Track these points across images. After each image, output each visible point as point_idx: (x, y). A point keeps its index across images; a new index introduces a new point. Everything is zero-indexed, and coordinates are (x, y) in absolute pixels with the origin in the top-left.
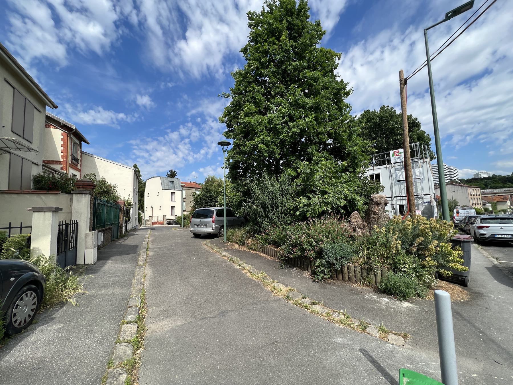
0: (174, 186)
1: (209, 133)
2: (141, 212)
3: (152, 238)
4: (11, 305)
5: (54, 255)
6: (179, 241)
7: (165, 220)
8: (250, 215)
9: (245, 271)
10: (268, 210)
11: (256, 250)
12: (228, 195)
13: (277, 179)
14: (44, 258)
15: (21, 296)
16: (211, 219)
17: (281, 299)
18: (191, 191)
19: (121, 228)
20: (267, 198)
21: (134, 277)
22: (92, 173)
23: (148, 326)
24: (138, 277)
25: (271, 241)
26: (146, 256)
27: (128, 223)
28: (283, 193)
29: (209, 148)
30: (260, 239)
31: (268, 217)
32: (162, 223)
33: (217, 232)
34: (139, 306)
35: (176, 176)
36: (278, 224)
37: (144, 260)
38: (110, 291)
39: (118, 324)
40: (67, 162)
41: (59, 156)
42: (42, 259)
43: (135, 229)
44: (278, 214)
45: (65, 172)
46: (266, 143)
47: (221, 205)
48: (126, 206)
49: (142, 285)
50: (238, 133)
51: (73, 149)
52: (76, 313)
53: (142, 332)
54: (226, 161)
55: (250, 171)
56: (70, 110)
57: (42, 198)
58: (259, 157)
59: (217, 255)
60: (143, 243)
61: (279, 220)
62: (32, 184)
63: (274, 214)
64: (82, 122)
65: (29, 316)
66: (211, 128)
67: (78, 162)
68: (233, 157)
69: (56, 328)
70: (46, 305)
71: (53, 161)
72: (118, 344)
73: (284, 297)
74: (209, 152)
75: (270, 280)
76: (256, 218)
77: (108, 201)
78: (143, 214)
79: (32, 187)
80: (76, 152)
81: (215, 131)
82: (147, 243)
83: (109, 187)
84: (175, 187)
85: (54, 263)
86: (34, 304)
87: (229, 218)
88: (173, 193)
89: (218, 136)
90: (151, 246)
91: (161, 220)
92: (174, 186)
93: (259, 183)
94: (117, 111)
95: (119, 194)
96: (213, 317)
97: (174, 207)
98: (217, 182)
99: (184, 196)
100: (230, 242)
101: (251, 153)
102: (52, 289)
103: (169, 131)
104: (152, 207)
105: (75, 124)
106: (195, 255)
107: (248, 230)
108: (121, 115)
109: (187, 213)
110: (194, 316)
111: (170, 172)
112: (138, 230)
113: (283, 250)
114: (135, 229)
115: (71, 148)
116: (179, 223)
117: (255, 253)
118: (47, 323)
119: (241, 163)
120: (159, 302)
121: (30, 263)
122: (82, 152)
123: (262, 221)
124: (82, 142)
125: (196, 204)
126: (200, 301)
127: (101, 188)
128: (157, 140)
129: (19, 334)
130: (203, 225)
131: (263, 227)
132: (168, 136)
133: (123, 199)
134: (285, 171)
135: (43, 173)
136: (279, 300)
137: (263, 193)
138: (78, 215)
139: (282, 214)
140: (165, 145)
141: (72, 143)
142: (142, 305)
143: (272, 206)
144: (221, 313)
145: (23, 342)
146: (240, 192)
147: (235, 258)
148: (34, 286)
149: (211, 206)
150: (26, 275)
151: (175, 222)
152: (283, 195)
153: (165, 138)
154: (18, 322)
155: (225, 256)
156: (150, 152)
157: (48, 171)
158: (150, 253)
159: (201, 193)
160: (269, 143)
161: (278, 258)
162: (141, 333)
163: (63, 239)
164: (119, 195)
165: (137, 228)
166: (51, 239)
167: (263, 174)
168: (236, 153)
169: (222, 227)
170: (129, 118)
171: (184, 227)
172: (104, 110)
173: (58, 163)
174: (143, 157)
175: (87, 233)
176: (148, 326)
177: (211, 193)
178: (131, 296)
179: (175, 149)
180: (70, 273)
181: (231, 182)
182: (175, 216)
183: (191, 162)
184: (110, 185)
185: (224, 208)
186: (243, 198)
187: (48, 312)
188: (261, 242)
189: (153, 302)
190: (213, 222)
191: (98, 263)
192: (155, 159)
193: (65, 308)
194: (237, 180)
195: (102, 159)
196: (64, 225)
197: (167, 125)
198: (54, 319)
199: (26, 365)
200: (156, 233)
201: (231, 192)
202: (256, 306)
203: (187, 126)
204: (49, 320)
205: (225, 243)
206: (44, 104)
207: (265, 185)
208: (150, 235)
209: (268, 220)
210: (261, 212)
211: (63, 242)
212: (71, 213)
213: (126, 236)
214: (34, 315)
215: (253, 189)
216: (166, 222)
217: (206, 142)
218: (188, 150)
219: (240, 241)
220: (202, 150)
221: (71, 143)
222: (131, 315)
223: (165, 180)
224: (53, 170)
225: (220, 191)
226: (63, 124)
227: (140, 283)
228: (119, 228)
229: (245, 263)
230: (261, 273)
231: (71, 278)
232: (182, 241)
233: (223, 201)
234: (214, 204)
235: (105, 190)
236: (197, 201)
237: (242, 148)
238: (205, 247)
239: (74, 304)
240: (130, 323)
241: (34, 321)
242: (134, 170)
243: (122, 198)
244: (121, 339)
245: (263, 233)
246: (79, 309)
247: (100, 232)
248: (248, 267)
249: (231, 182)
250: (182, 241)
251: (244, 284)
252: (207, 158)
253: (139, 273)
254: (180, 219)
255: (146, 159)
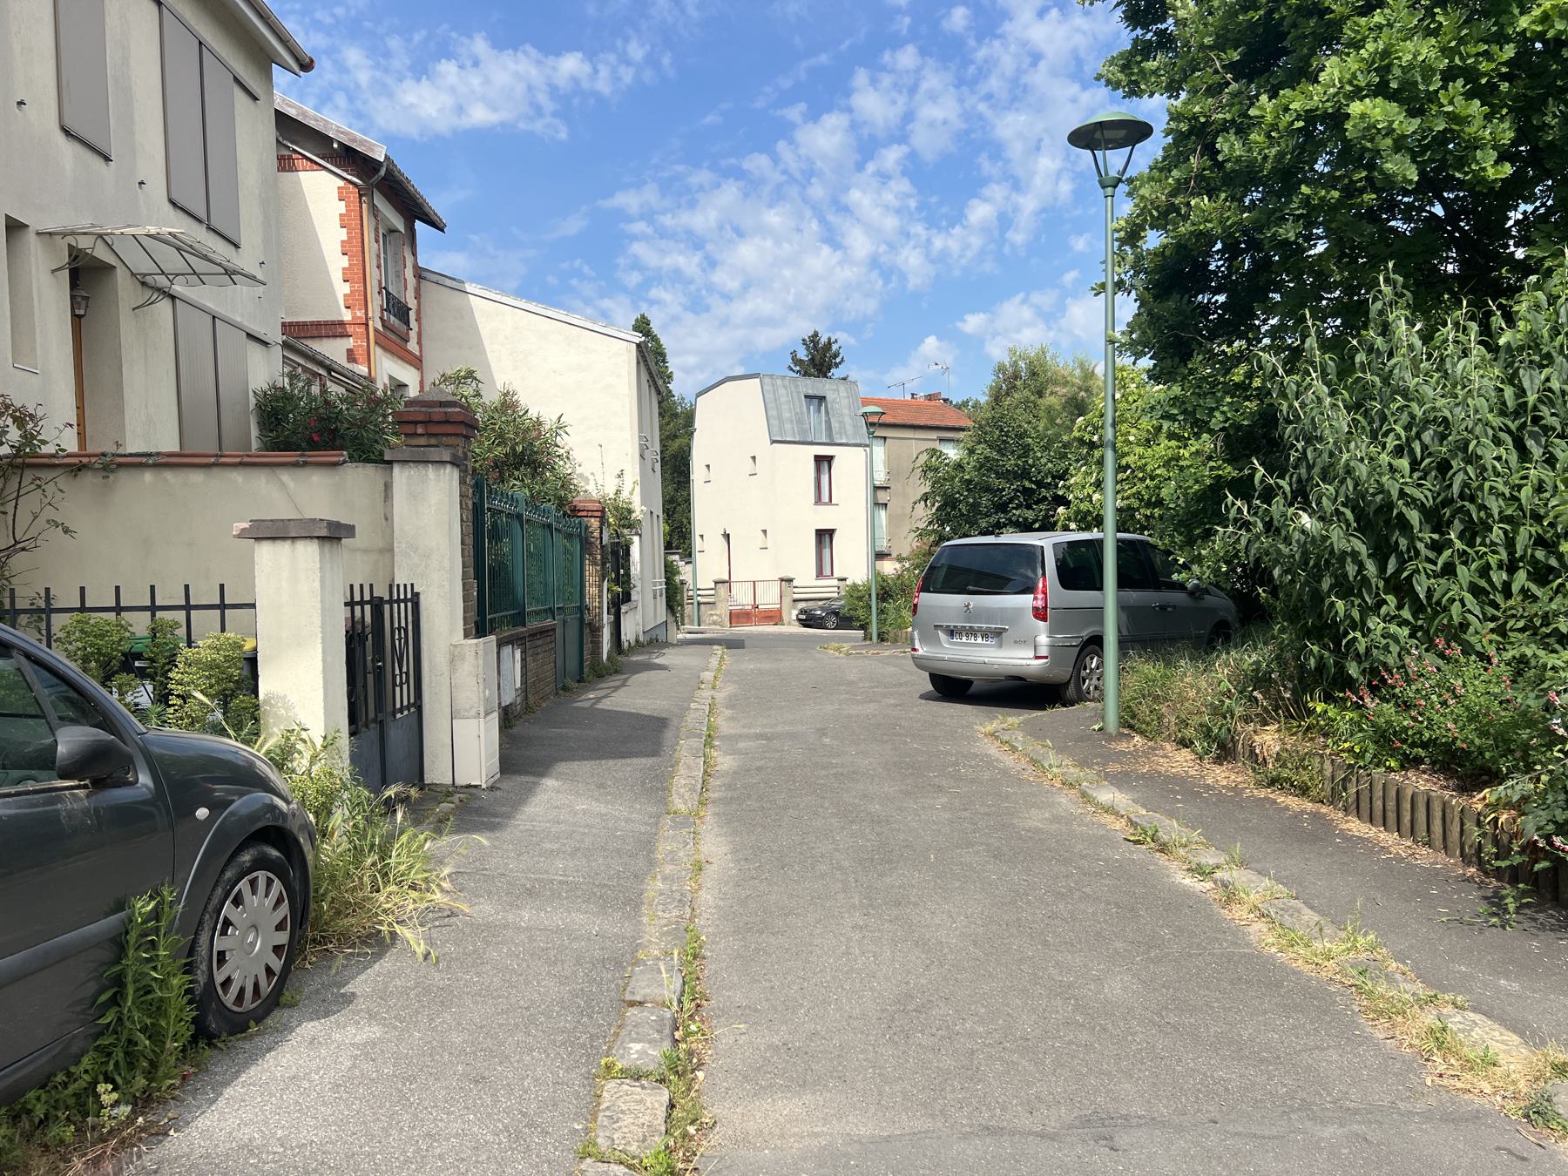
0: (828, 422)
1: (1018, 93)
2: (676, 557)
3: (730, 689)
4: (207, 916)
5: (338, 731)
6: (855, 710)
7: (787, 601)
8: (1276, 572)
9: (1239, 913)
10: (1403, 543)
11: (1313, 793)
12: (1130, 459)
13: (1487, 332)
14: (304, 741)
15: (237, 889)
16: (1026, 601)
17: (1488, 1114)
18: (915, 447)
19: (596, 631)
20: (1404, 463)
21: (652, 863)
22: (460, 367)
23: (715, 1110)
24: (668, 869)
25: (1424, 745)
26: (705, 772)
27: (624, 608)
28: (1524, 425)
29: (1017, 185)
30: (1344, 727)
31: (1402, 588)
32: (774, 617)
33: (1063, 673)
34: (675, 1007)
35: (837, 365)
36: (1481, 635)
37: (692, 790)
38: (554, 917)
39: (589, 1072)
40: (367, 325)
41: (337, 301)
42: (300, 746)
43: (653, 642)
44: (1484, 571)
45: (362, 369)
46: (1408, 85)
47: (1083, 519)
48: (609, 525)
49: (688, 910)
50: (1202, 47)
51: (385, 259)
52: (427, 991)
53: (691, 1130)
54: (1123, 242)
55: (1277, 297)
56: (364, 77)
57: (283, 485)
58: (1350, 191)
59: (1066, 801)
60: (689, 709)
61: (1491, 611)
62: (254, 432)
63: (1449, 570)
64: (413, 131)
65: (269, 971)
66: (1028, 60)
67: (407, 323)
68: (1164, 216)
69: (358, 1039)
70: (322, 937)
71: (318, 324)
72: (589, 1160)
73: (1511, 1104)
74: (1016, 209)
75: (1408, 986)
76: (1318, 597)
77: (533, 501)
78: (689, 567)
79: (255, 444)
80: (398, 276)
81: (1054, 73)
82: (707, 708)
83: (534, 434)
84: (835, 425)
85: (342, 766)
86: (280, 927)
87: (1134, 596)
88: (823, 462)
89: (1074, 100)
90: (724, 725)
91: (769, 598)
92: (828, 422)
93: (1346, 368)
94: (552, 48)
95: (579, 470)
96: (1042, 1136)
97: (831, 532)
98: (1066, 383)
99: (880, 478)
100: (1142, 733)
101: (1287, 176)
102: (340, 875)
103: (794, 113)
104: (727, 537)
105: (387, 139)
106: (940, 788)
107: (1257, 670)
108: (571, 64)
109: (898, 566)
110: (938, 1107)
111: (808, 348)
112: (667, 644)
113: (1509, 805)
114: (653, 642)
115: (379, 256)
116: (858, 619)
117: (1303, 812)
118: (327, 1015)
119: (1219, 246)
120: (766, 1005)
121: (258, 753)
122: (420, 274)
123: (1356, 614)
124: (418, 225)
125: (942, 517)
126: (971, 1035)
127: (501, 438)
128: (738, 174)
129: (239, 1036)
130: (980, 630)
131: (1362, 650)
132: (791, 141)
133: (595, 495)
134: (1549, 273)
135: (286, 380)
136: (1477, 1116)
137: (1374, 435)
138: (416, 560)
139: (1512, 569)
140: (778, 197)
141: (381, 231)
142: (686, 1006)
143: (1435, 519)
144: (1086, 1122)
145: (253, 1071)
146: (1211, 432)
147: (1171, 829)
148: (275, 853)
149: (1026, 527)
150: (246, 803)
151: (836, 614)
152: (1530, 443)
153: (776, 160)
154: (234, 990)
155: (1110, 810)
156: (709, 247)
157: (305, 369)
158: (725, 762)
159: (971, 452)
160: (1427, 80)
161: (1473, 856)
162: (685, 1135)
163: (369, 664)
164: (581, 475)
165: (662, 638)
166: (324, 661)
167: (1379, 305)
168: (1187, 181)
169: (1094, 643)
170: (604, 72)
171: (882, 638)
172: (495, 52)
173: (335, 330)
174: (677, 277)
175: (455, 646)
176: (715, 1110)
177: (1027, 450)
178: (641, 955)
179: (831, 218)
180: (399, 815)
181: (1155, 376)
182: (835, 582)
183: (914, 282)
184: (539, 423)
185: (1109, 536)
186: (1229, 471)
187: (330, 967)
188: (1351, 750)
189: (738, 997)
190: (1040, 614)
191: (504, 785)
192: (733, 285)
193: (385, 964)
194: (1186, 357)
195: (498, 298)
196: (367, 603)
197: (786, 83)
198: (351, 1002)
199: (264, 1163)
200: (747, 663)
201: (1147, 443)
202: (1309, 1124)
203: (892, 71)
204: (335, 1002)
205: (1110, 738)
206: (263, 59)
207: (1386, 380)
208: (719, 670)
209: (1400, 607)
210: (1355, 554)
211: (370, 678)
212: (391, 550)
213: (616, 672)
214: (286, 970)
215: (1303, 405)
216: (795, 612)
217: (997, 150)
218: (898, 212)
219: (1207, 733)
220: (974, 202)
221: (376, 230)
222: (639, 1041)
223: (782, 391)
224: (321, 364)
225: (1081, 441)
226: (339, 143)
227: (677, 896)
228: (587, 631)
229: (1243, 864)
230: (1343, 935)
231: (404, 838)
232: (871, 709)
233: (1096, 497)
234: (1047, 517)
235: (519, 449)
236: (949, 503)
237: (1229, 146)
238: (993, 749)
239: (420, 950)
240: (637, 1076)
241: (287, 996)
242: (638, 346)
243: (591, 488)
244: (599, 1141)
245: (1364, 691)
246: (437, 976)
247: (508, 643)
248: (1255, 887)
249: (1155, 376)
250: (871, 709)
251: (1232, 983)
252: (1006, 250)
253: (671, 852)
254: (860, 598)
255: (693, 288)
